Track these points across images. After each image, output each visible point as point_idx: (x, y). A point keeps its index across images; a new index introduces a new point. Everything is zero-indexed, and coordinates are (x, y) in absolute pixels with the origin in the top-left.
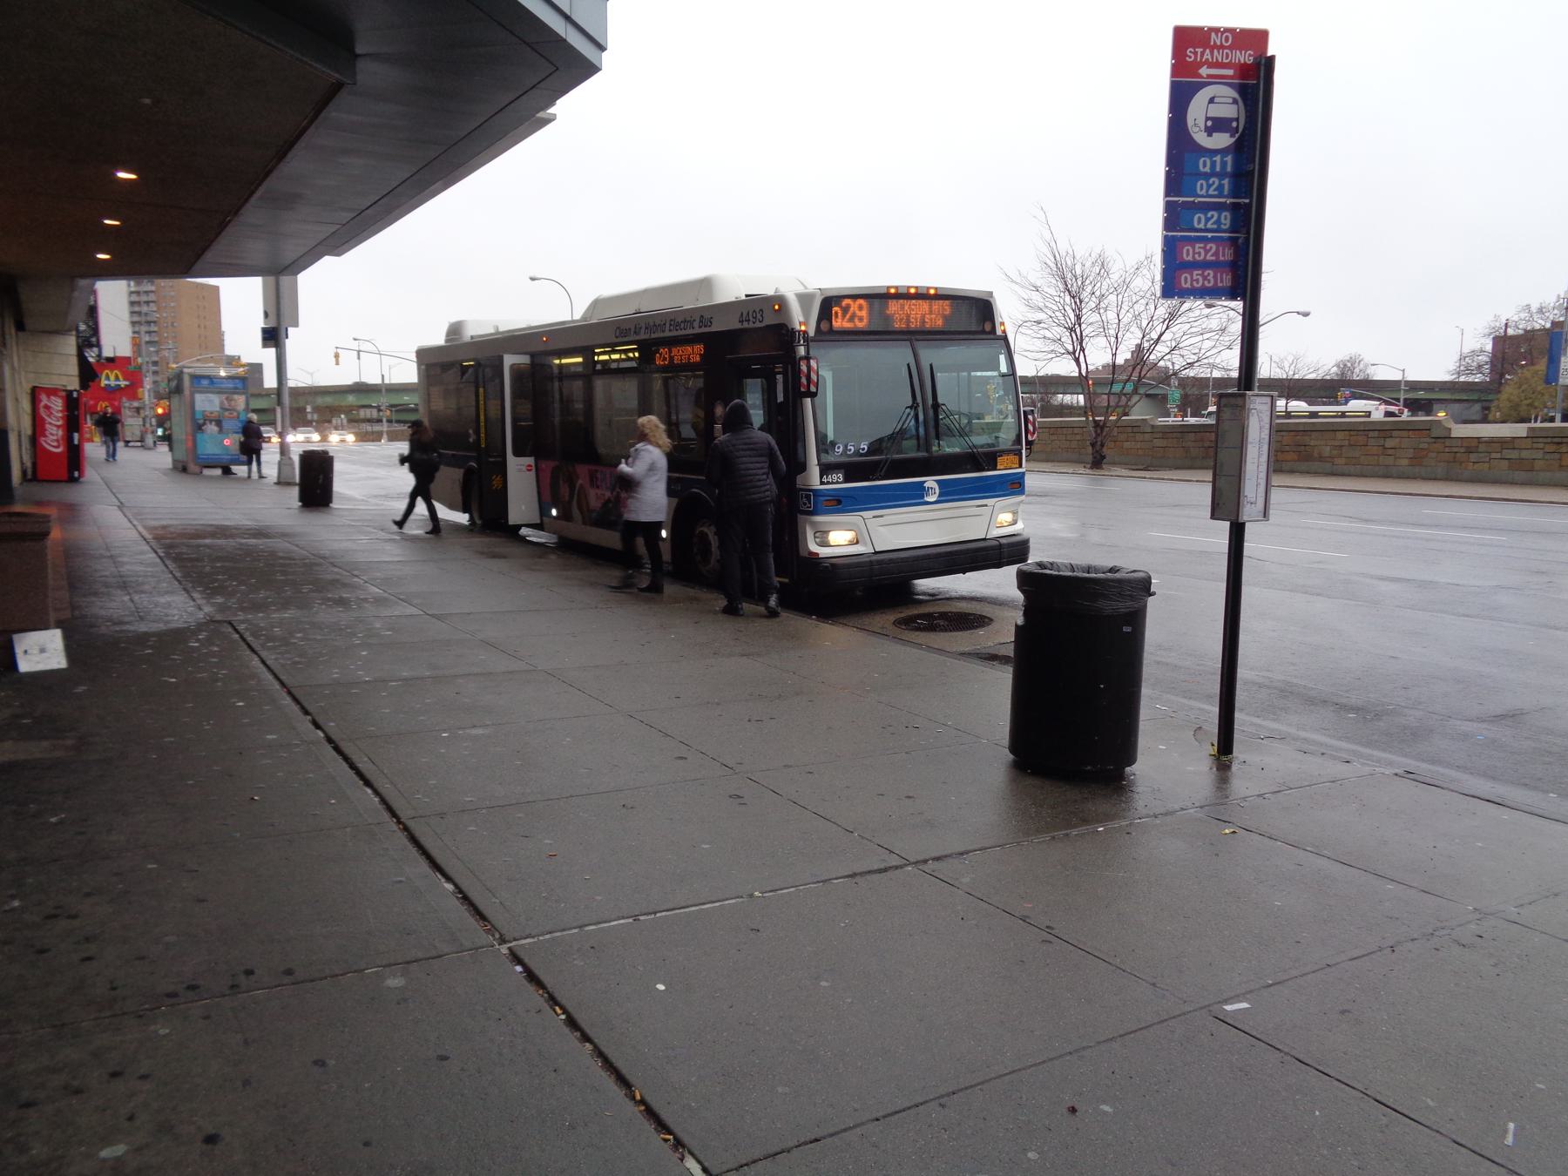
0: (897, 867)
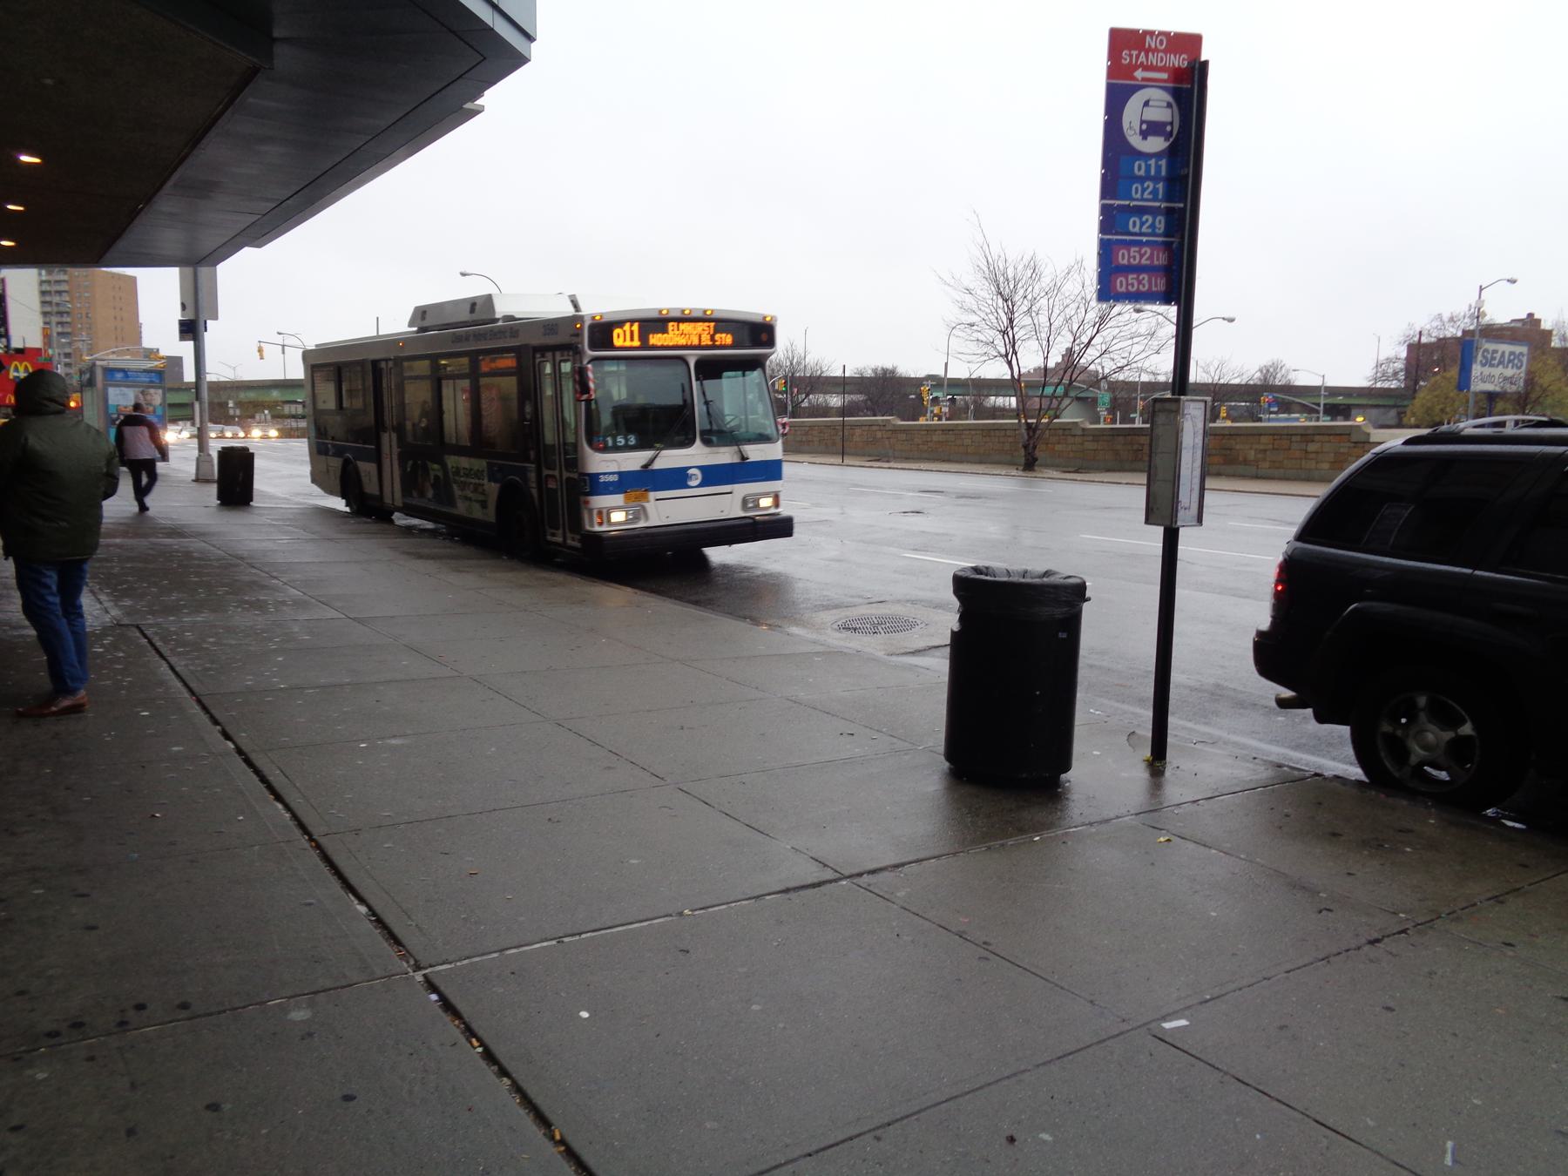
0: (830, 881)
